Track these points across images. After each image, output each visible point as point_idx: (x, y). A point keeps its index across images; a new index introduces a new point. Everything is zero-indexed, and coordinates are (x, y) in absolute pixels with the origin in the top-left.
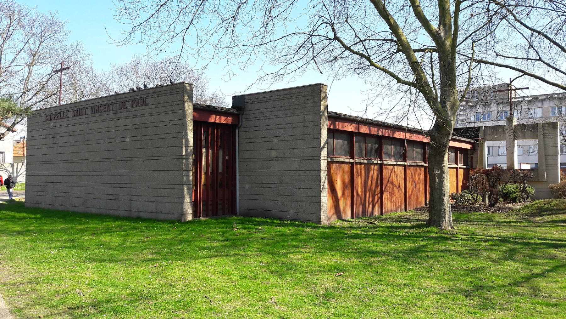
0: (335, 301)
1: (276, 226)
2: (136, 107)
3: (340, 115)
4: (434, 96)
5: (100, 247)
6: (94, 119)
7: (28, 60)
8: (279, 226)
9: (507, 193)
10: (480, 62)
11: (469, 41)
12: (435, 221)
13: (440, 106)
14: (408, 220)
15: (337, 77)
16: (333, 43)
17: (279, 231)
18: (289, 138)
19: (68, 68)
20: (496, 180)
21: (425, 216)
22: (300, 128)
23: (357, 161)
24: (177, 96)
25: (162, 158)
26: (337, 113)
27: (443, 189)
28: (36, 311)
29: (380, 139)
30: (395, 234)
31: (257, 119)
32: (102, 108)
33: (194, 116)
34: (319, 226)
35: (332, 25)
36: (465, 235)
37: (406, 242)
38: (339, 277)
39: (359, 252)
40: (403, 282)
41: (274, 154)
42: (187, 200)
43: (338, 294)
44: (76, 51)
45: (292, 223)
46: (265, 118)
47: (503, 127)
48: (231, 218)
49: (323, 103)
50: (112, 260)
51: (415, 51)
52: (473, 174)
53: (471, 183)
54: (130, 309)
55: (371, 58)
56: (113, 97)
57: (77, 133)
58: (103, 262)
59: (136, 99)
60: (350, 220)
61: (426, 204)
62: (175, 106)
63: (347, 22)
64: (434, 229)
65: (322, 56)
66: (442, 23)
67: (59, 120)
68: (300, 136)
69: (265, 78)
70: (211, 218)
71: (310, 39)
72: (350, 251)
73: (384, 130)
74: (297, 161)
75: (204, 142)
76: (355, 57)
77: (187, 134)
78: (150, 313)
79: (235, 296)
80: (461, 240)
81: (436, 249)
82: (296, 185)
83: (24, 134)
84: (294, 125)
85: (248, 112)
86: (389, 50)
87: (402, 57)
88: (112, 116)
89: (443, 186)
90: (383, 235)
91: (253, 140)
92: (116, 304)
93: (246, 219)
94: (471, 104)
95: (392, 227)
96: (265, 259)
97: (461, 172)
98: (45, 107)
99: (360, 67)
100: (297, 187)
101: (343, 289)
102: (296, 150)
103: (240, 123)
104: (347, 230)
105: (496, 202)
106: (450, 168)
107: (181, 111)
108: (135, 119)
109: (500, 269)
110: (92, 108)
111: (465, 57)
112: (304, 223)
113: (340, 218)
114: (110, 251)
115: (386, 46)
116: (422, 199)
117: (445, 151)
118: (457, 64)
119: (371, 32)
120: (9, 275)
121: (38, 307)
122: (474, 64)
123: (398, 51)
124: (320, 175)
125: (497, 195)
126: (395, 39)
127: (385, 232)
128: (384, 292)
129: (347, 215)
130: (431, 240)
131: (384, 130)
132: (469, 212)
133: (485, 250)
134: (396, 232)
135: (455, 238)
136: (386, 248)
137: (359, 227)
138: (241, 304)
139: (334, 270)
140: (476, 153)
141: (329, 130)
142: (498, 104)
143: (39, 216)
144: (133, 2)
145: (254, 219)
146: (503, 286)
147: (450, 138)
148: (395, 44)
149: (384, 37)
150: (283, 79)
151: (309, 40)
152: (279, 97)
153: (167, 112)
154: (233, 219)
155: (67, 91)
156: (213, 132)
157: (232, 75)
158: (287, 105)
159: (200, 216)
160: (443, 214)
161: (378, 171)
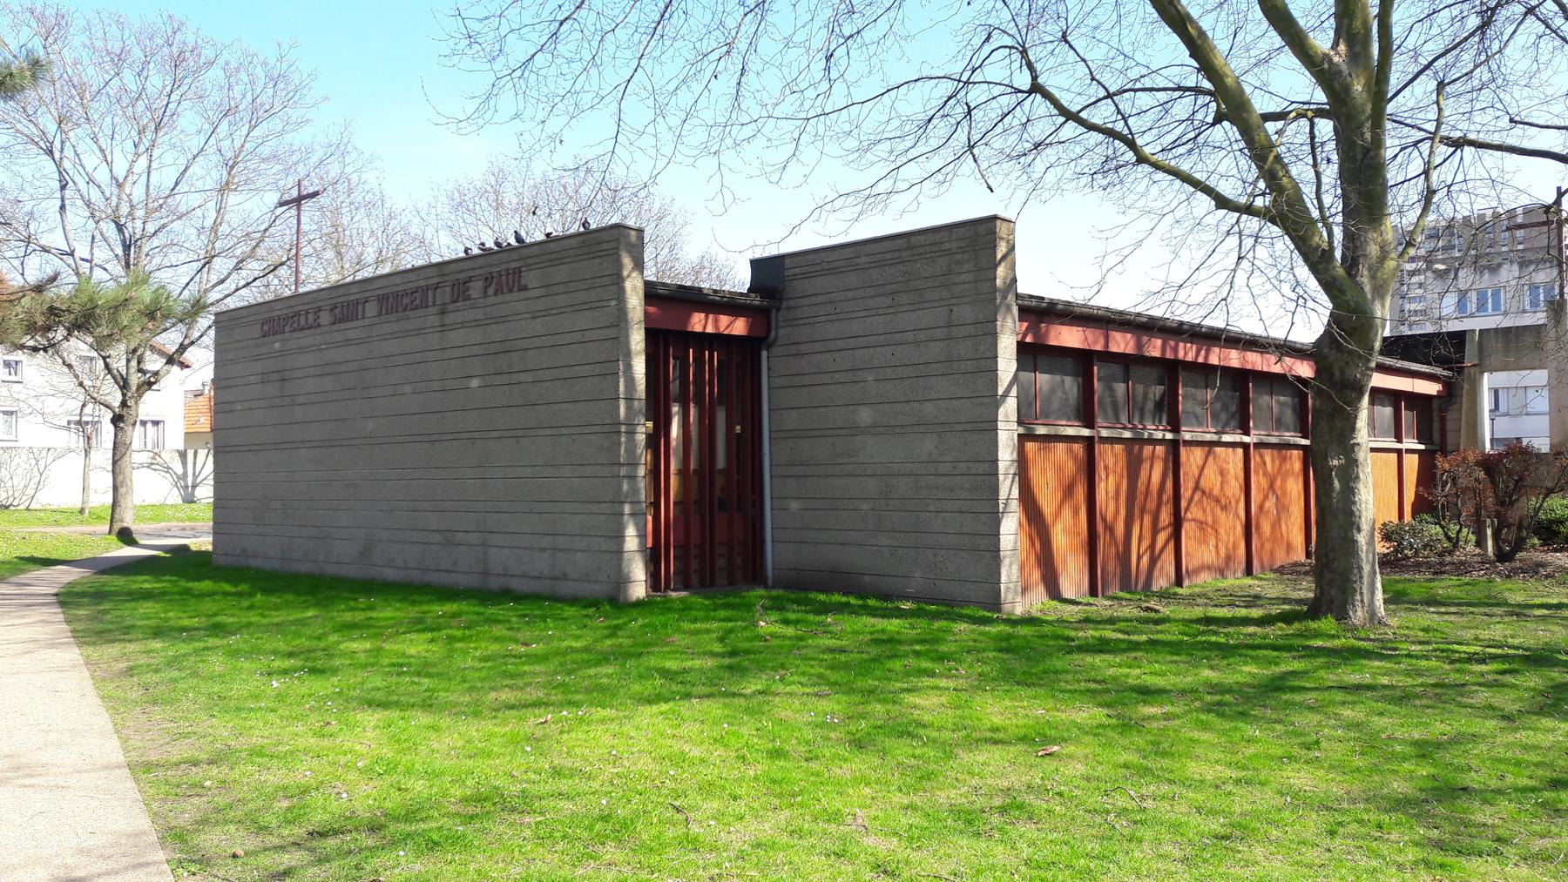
0: (1033, 826)
1: (875, 616)
2: (496, 294)
3: (1053, 304)
4: (1325, 246)
5: (400, 670)
6: (386, 329)
7: (217, 176)
8: (883, 617)
9: (1551, 522)
10: (1458, 144)
11: (1426, 84)
12: (1332, 602)
13: (1341, 271)
14: (1254, 600)
15: (1039, 192)
16: (1027, 103)
17: (883, 631)
18: (909, 371)
19: (315, 194)
20: (1516, 486)
21: (1306, 590)
22: (939, 343)
23: (1104, 433)
24: (601, 263)
25: (565, 431)
26: (1043, 298)
27: (1355, 509)
28: (227, 840)
29: (1170, 370)
30: (1214, 639)
31: (820, 319)
32: (406, 301)
33: (646, 313)
34: (995, 616)
35: (1024, 53)
36: (1421, 643)
37: (1245, 663)
38: (1048, 757)
39: (1108, 691)
40: (1233, 776)
41: (865, 416)
42: (631, 542)
43: (1045, 806)
44: (339, 149)
45: (919, 609)
46: (842, 316)
47: (1537, 329)
48: (751, 594)
49: (1001, 271)
50: (430, 706)
51: (1268, 117)
52: (1447, 466)
53: (1441, 494)
54: (471, 837)
55: (1139, 142)
56: (434, 269)
57: (344, 368)
58: (407, 710)
59: (495, 274)
60: (1084, 601)
61: (1308, 555)
62: (598, 290)
63: (1067, 42)
64: (1327, 624)
65: (997, 143)
66: (1343, 34)
67: (296, 334)
68: (939, 365)
69: (838, 204)
70: (695, 594)
71: (963, 93)
72: (1083, 685)
73: (1181, 345)
74: (929, 435)
75: (675, 387)
76: (1092, 142)
77: (629, 367)
78: (523, 850)
79: (756, 805)
80: (1409, 656)
81: (1334, 681)
82: (930, 501)
83: (208, 374)
84: (922, 336)
85: (792, 303)
86: (1191, 119)
87: (1230, 134)
88: (434, 321)
89: (1354, 503)
90: (1181, 642)
91: (807, 380)
92: (434, 825)
93: (792, 596)
94: (1441, 267)
95: (1208, 621)
96: (833, 705)
97: (1411, 462)
98: (262, 300)
99: (1109, 166)
100: (931, 508)
101: (1057, 794)
102: (928, 404)
103: (773, 334)
104: (1076, 629)
105: (1519, 545)
106: (1373, 450)
107: (613, 303)
108: (494, 326)
109: (1524, 739)
110: (382, 299)
111: (1414, 131)
112: (948, 605)
113: (1054, 592)
114: (426, 680)
115: (1183, 107)
116: (1298, 539)
117: (1359, 399)
118: (1389, 153)
119: (1141, 68)
120: (162, 742)
121: (232, 828)
122: (1443, 150)
123: (1218, 120)
124: (997, 475)
125: (1520, 528)
126: (1207, 85)
127: (1186, 635)
128: (1175, 803)
129: (1072, 580)
130: (1318, 656)
131: (1181, 345)
132: (1435, 577)
133: (1480, 684)
134: (1216, 633)
135: (1390, 652)
136: (1189, 679)
137: (1111, 621)
138: (771, 829)
139: (1034, 740)
140: (1456, 406)
141: (1022, 347)
142: (1523, 264)
143: (243, 587)
144: (486, 18)
145: (812, 595)
146: (1533, 789)
147: (1373, 365)
148: (1208, 98)
149: (1176, 80)
150: (886, 206)
151: (958, 96)
152: (877, 258)
153: (576, 308)
154: (756, 597)
155: (317, 254)
156: (699, 360)
157: (729, 198)
158: (900, 279)
159: (667, 587)
160: (1356, 582)
161: (1166, 461)
